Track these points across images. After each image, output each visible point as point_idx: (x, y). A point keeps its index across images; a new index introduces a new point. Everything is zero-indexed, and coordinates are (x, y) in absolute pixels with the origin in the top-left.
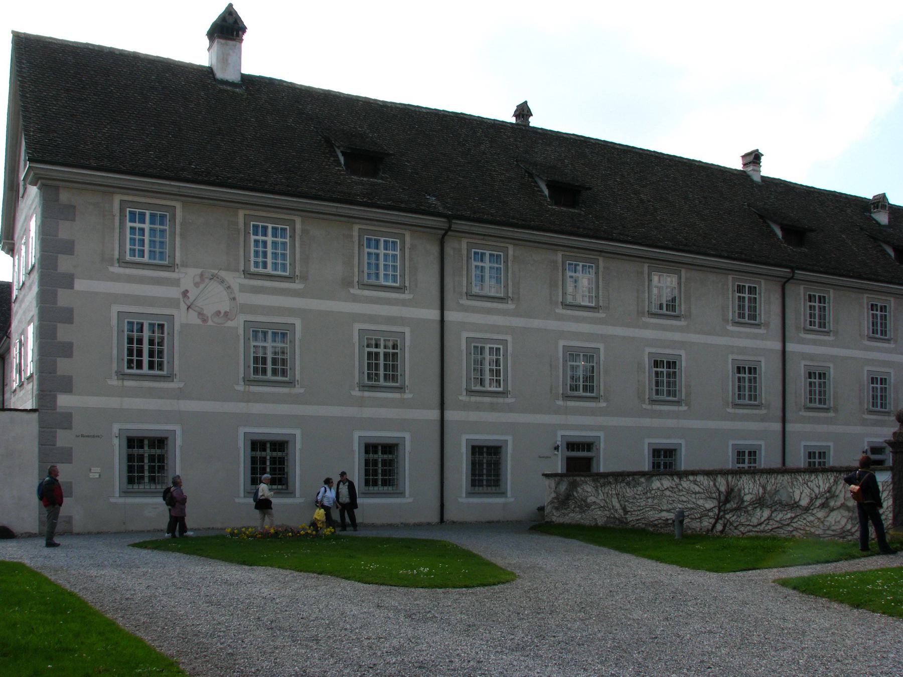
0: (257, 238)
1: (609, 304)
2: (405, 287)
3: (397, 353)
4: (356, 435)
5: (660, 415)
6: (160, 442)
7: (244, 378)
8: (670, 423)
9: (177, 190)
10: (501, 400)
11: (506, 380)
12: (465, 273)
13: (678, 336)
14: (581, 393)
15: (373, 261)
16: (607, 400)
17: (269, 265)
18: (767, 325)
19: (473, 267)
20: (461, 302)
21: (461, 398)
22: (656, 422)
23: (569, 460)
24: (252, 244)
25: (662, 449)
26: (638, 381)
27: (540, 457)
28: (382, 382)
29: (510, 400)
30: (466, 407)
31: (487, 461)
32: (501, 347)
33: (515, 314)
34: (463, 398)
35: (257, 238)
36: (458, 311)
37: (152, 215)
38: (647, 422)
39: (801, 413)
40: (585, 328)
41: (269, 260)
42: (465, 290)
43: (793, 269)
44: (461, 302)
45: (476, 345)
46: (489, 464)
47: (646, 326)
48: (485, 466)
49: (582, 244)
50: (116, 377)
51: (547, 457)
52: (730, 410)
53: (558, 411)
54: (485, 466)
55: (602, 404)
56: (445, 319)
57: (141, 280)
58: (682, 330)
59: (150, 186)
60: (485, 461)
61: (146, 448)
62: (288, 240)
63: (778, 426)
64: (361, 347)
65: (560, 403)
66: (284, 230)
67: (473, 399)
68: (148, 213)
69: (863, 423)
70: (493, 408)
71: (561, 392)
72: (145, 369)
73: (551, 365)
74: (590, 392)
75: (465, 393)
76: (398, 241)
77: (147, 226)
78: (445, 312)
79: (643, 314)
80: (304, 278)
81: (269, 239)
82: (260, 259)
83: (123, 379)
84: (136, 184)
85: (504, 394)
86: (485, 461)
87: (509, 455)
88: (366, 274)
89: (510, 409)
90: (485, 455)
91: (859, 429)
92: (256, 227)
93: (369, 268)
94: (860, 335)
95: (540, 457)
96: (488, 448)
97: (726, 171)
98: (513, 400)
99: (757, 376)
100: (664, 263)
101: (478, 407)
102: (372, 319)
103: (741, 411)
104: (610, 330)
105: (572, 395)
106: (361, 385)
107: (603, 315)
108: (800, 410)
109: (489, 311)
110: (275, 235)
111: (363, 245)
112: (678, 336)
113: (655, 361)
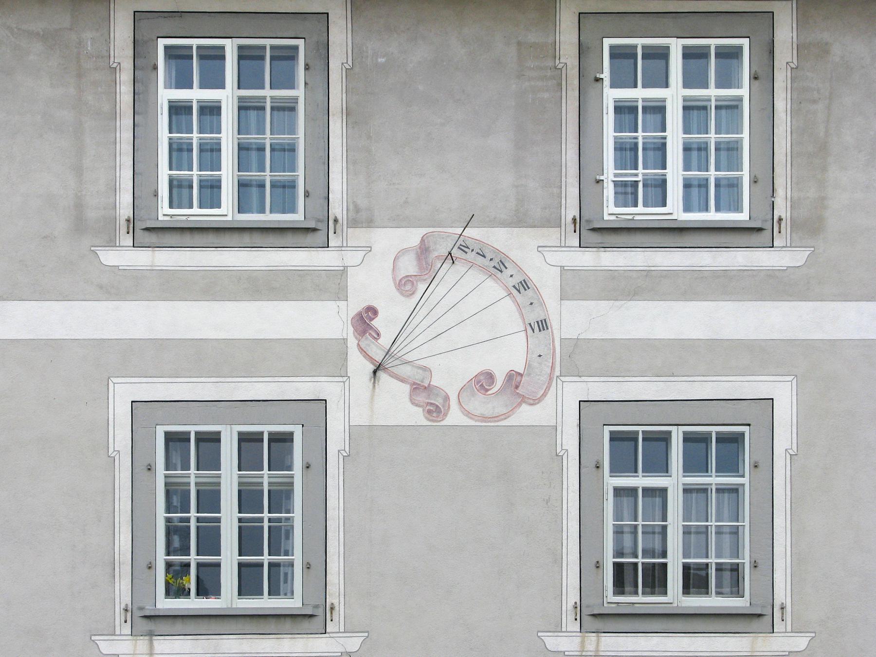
37: (245, 55)
66: (734, 54)
83: (151, 634)
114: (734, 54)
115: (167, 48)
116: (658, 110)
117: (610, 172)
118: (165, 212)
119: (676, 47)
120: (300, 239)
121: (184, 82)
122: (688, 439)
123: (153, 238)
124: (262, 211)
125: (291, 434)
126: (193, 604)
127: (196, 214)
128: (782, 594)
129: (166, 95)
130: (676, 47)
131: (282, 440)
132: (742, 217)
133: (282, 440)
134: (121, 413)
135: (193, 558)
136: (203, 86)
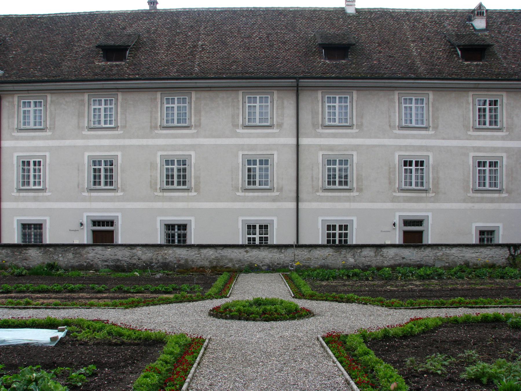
0: (329, 104)
1: (126, 124)
2: (274, 125)
3: (497, 169)
4: (241, 219)
5: (171, 199)
6: (183, 227)
7: (472, 189)
8: (180, 205)
9: (12, 88)
10: (41, 194)
11: (44, 181)
12: (16, 116)
13: (188, 141)
14: (337, 186)
15: (408, 112)
16: (123, 190)
17: (337, 120)
18: (280, 126)
19: (327, 106)
20: (13, 134)
21: (13, 194)
22: (167, 205)
23: (405, 233)
24: (327, 109)
25: (176, 224)
26: (151, 176)
27: (70, 230)
28: (487, 187)
29: (47, 194)
30: (16, 199)
31: (34, 233)
32: (41, 160)
33: (52, 138)
34: (15, 194)
35: (329, 104)
36: (11, 140)
37: (105, 101)
38: (158, 205)
39: (318, 194)
40: (106, 142)
41: (337, 117)
42: (16, 127)
43: (298, 79)
44: (13, 134)
45: (24, 160)
46: (35, 235)
47: (320, 136)
48: (33, 237)
49: (286, 84)
50: (87, 191)
51: (76, 230)
52: (240, 194)
53: (84, 200)
54: (33, 237)
55: (120, 194)
56: (300, 143)
57: (335, 136)
58: (192, 136)
59: (383, 84)
60: (33, 233)
61: (176, 230)
62: (187, 105)
63: (293, 205)
64: (324, 165)
65: (86, 194)
66: (41, 102)
67: (22, 194)
68: (414, 98)
69: (394, 200)
70: (35, 199)
71: (86, 187)
72: (103, 186)
73: (78, 170)
74: (27, 186)
75: (15, 191)
76: (269, 96)
77: (337, 105)
78: (299, 139)
79: (156, 128)
80: (124, 127)
81: (413, 105)
82: (97, 119)
83: (163, 192)
84: (80, 86)
85: (43, 190)
86: (33, 233)
87: (47, 230)
88: (92, 122)
89: (48, 199)
90: (33, 229)
91: (389, 205)
92: (24, 103)
93: (94, 118)
94: (390, 126)
95: (70, 230)
96: (35, 225)
97: (19, 18)
98: (50, 194)
99: (348, 166)
100: (185, 89)
101: (25, 199)
102: (406, 148)
103: (251, 194)
104: (127, 142)
105: (249, 188)
106: (323, 188)
107: (121, 132)
108: (317, 191)
109: (33, 138)
110: (417, 103)
111: (325, 102)
112: (188, 141)
113: (404, 161)
114: (41, 102)
115: (23, 102)
116: (334, 107)
117: (327, 117)
118: (327, 123)
119: (32, 101)
120: (270, 128)
121: (168, 103)
122: (177, 161)
123: (20, 131)
124: (342, 123)
125: (33, 161)
126: (108, 187)
127: (332, 123)
128: (119, 186)
129: (247, 105)
130: (32, 101)
131: (40, 162)
132: (348, 124)
133: (40, 162)
134: (15, 159)
135: (182, 180)
136: (253, 103)
